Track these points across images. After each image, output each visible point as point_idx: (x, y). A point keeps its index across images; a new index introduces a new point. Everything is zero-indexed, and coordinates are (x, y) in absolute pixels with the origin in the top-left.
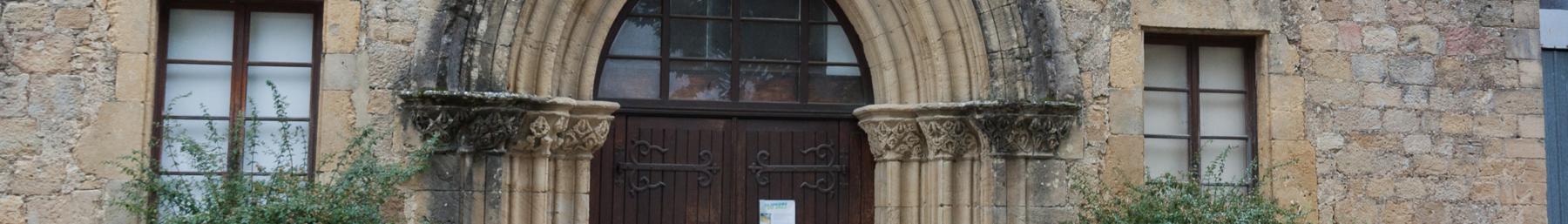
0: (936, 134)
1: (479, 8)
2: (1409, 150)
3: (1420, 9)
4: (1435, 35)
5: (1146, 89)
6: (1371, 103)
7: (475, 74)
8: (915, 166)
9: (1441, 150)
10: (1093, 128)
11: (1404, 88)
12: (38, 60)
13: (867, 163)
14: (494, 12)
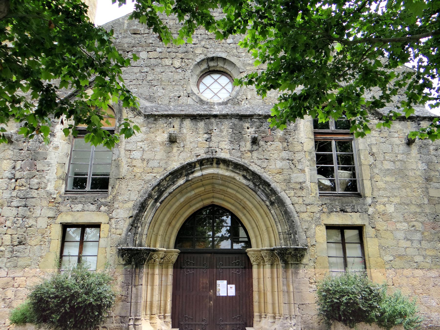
0: (266, 257)
1: (139, 225)
2: (416, 261)
3: (414, 217)
4: (420, 225)
5: (328, 243)
6: (401, 246)
7: (137, 242)
8: (262, 266)
9: (427, 260)
10: (312, 254)
11: (412, 241)
12: (33, 242)
13: (250, 266)
14: (143, 225)
